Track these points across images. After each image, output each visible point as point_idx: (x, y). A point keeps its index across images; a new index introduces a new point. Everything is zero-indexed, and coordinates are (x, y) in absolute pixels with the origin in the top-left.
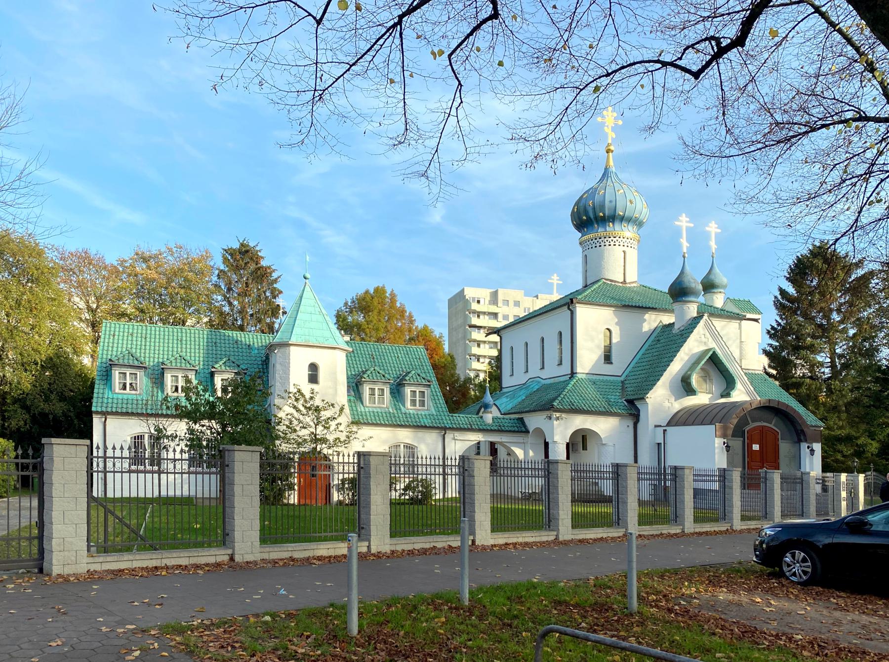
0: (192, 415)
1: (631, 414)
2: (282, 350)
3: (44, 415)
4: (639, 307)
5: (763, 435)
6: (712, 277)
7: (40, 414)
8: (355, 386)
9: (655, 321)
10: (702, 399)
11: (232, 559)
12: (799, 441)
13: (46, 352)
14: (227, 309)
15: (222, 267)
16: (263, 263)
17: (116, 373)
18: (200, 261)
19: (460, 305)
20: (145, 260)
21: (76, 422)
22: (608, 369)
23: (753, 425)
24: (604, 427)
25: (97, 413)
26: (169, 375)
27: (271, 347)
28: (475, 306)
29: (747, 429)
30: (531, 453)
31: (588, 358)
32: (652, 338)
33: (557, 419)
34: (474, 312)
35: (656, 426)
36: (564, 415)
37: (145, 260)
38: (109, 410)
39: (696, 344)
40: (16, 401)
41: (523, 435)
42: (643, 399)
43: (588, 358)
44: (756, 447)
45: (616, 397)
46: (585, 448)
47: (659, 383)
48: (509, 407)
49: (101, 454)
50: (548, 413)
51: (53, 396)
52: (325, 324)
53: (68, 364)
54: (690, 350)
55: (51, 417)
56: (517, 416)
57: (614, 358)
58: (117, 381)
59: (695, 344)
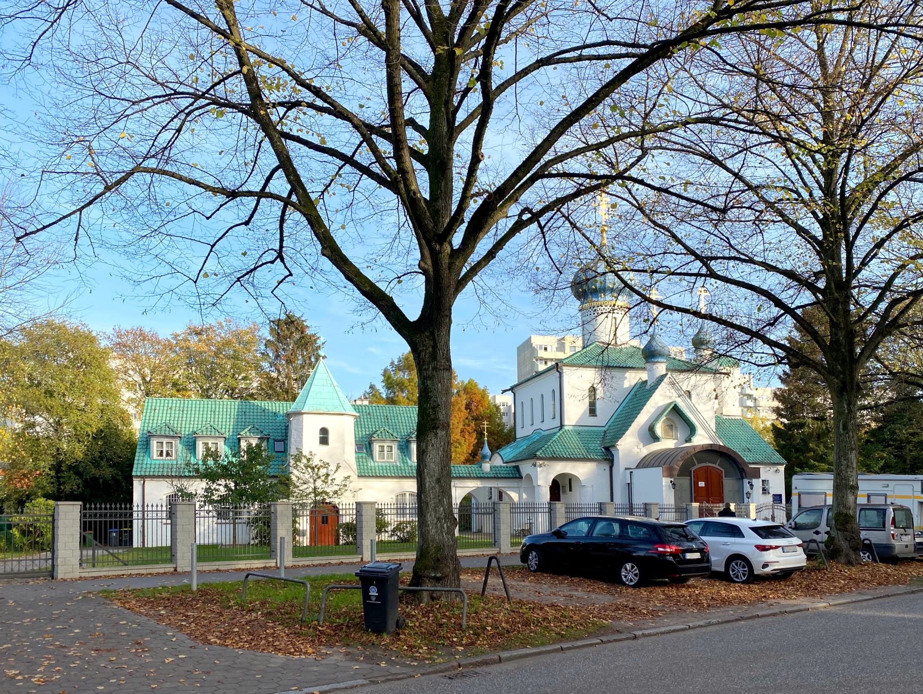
0: (211, 476)
1: (606, 460)
2: (297, 418)
3: (95, 479)
4: (619, 367)
5: (707, 475)
6: (654, 343)
7: (91, 479)
8: (365, 445)
9: (634, 378)
10: (667, 444)
11: (176, 570)
12: (742, 478)
13: (96, 424)
14: (274, 375)
15: (270, 338)
16: (308, 332)
17: (154, 443)
18: (247, 333)
19: (528, 353)
20: (198, 333)
21: (124, 484)
22: (592, 421)
23: (698, 466)
24: (582, 471)
25: (137, 477)
26: (201, 443)
27: (288, 415)
28: (541, 354)
29: (693, 469)
30: (524, 496)
31: (575, 411)
32: (632, 393)
33: (540, 466)
34: (542, 359)
35: (626, 469)
36: (546, 463)
37: (198, 333)
38: (147, 474)
39: (662, 398)
40: (70, 468)
41: (517, 480)
42: (614, 446)
43: (575, 411)
44: (702, 484)
45: (597, 445)
46: (570, 490)
47: (628, 433)
48: (510, 457)
49: (140, 508)
50: (532, 461)
51: (103, 463)
52: (335, 395)
53: (117, 434)
54: (656, 403)
55: (101, 481)
56: (514, 464)
57: (598, 412)
58: (155, 449)
59: (661, 398)
